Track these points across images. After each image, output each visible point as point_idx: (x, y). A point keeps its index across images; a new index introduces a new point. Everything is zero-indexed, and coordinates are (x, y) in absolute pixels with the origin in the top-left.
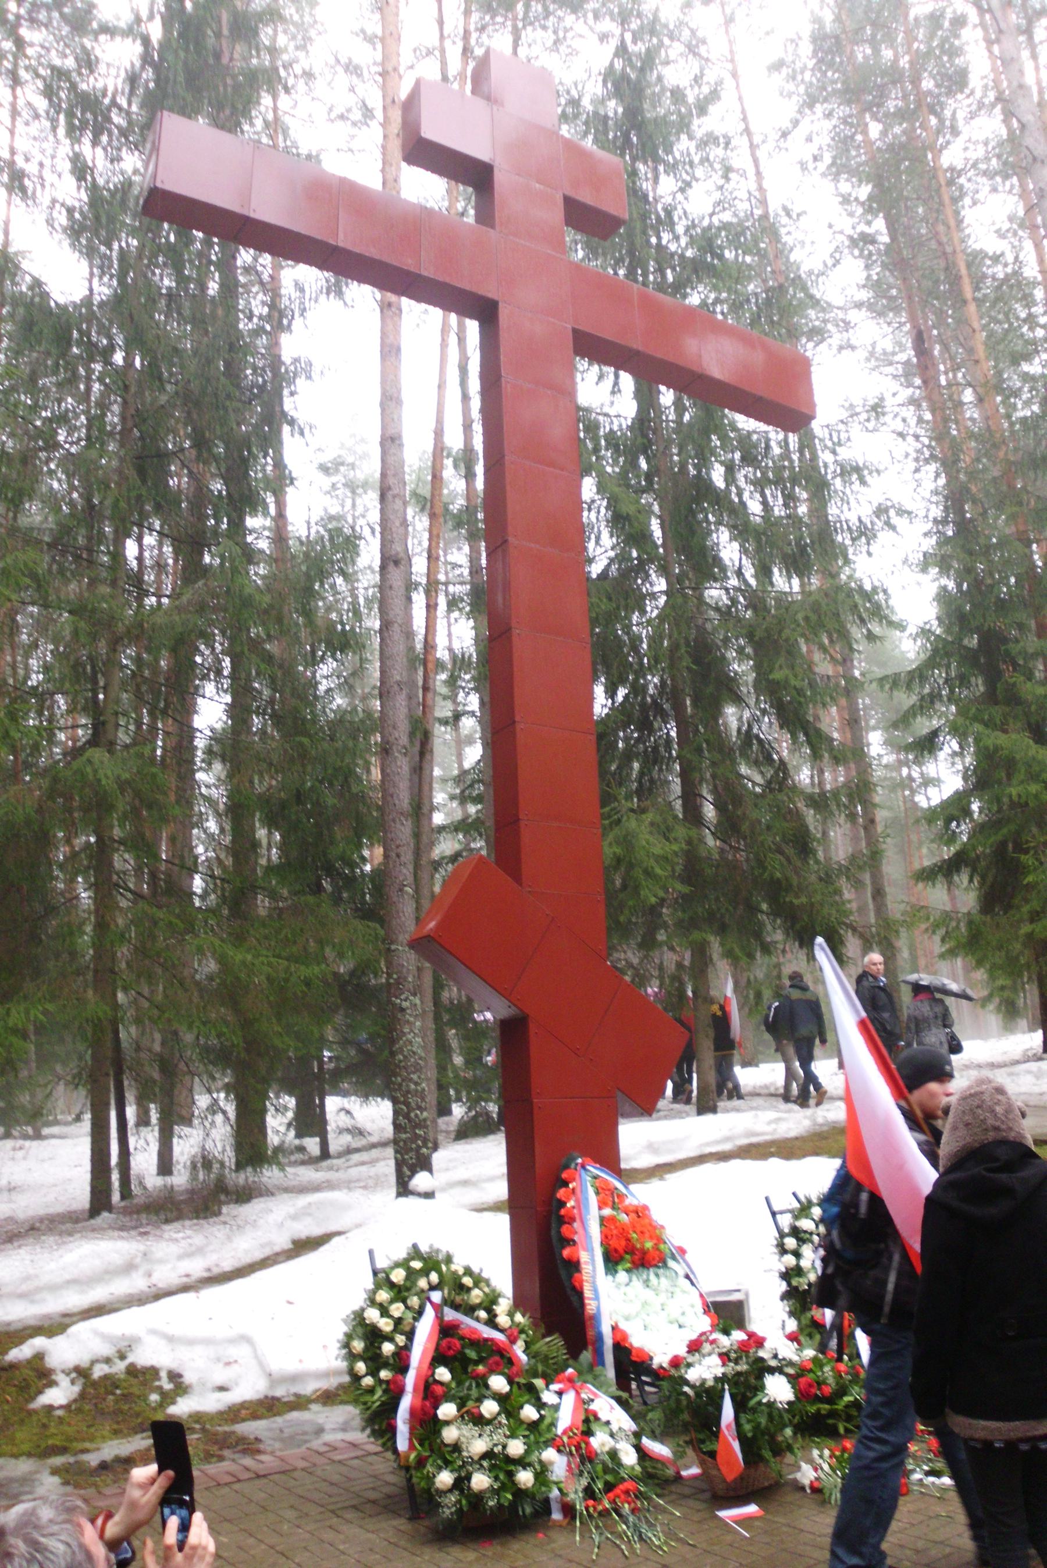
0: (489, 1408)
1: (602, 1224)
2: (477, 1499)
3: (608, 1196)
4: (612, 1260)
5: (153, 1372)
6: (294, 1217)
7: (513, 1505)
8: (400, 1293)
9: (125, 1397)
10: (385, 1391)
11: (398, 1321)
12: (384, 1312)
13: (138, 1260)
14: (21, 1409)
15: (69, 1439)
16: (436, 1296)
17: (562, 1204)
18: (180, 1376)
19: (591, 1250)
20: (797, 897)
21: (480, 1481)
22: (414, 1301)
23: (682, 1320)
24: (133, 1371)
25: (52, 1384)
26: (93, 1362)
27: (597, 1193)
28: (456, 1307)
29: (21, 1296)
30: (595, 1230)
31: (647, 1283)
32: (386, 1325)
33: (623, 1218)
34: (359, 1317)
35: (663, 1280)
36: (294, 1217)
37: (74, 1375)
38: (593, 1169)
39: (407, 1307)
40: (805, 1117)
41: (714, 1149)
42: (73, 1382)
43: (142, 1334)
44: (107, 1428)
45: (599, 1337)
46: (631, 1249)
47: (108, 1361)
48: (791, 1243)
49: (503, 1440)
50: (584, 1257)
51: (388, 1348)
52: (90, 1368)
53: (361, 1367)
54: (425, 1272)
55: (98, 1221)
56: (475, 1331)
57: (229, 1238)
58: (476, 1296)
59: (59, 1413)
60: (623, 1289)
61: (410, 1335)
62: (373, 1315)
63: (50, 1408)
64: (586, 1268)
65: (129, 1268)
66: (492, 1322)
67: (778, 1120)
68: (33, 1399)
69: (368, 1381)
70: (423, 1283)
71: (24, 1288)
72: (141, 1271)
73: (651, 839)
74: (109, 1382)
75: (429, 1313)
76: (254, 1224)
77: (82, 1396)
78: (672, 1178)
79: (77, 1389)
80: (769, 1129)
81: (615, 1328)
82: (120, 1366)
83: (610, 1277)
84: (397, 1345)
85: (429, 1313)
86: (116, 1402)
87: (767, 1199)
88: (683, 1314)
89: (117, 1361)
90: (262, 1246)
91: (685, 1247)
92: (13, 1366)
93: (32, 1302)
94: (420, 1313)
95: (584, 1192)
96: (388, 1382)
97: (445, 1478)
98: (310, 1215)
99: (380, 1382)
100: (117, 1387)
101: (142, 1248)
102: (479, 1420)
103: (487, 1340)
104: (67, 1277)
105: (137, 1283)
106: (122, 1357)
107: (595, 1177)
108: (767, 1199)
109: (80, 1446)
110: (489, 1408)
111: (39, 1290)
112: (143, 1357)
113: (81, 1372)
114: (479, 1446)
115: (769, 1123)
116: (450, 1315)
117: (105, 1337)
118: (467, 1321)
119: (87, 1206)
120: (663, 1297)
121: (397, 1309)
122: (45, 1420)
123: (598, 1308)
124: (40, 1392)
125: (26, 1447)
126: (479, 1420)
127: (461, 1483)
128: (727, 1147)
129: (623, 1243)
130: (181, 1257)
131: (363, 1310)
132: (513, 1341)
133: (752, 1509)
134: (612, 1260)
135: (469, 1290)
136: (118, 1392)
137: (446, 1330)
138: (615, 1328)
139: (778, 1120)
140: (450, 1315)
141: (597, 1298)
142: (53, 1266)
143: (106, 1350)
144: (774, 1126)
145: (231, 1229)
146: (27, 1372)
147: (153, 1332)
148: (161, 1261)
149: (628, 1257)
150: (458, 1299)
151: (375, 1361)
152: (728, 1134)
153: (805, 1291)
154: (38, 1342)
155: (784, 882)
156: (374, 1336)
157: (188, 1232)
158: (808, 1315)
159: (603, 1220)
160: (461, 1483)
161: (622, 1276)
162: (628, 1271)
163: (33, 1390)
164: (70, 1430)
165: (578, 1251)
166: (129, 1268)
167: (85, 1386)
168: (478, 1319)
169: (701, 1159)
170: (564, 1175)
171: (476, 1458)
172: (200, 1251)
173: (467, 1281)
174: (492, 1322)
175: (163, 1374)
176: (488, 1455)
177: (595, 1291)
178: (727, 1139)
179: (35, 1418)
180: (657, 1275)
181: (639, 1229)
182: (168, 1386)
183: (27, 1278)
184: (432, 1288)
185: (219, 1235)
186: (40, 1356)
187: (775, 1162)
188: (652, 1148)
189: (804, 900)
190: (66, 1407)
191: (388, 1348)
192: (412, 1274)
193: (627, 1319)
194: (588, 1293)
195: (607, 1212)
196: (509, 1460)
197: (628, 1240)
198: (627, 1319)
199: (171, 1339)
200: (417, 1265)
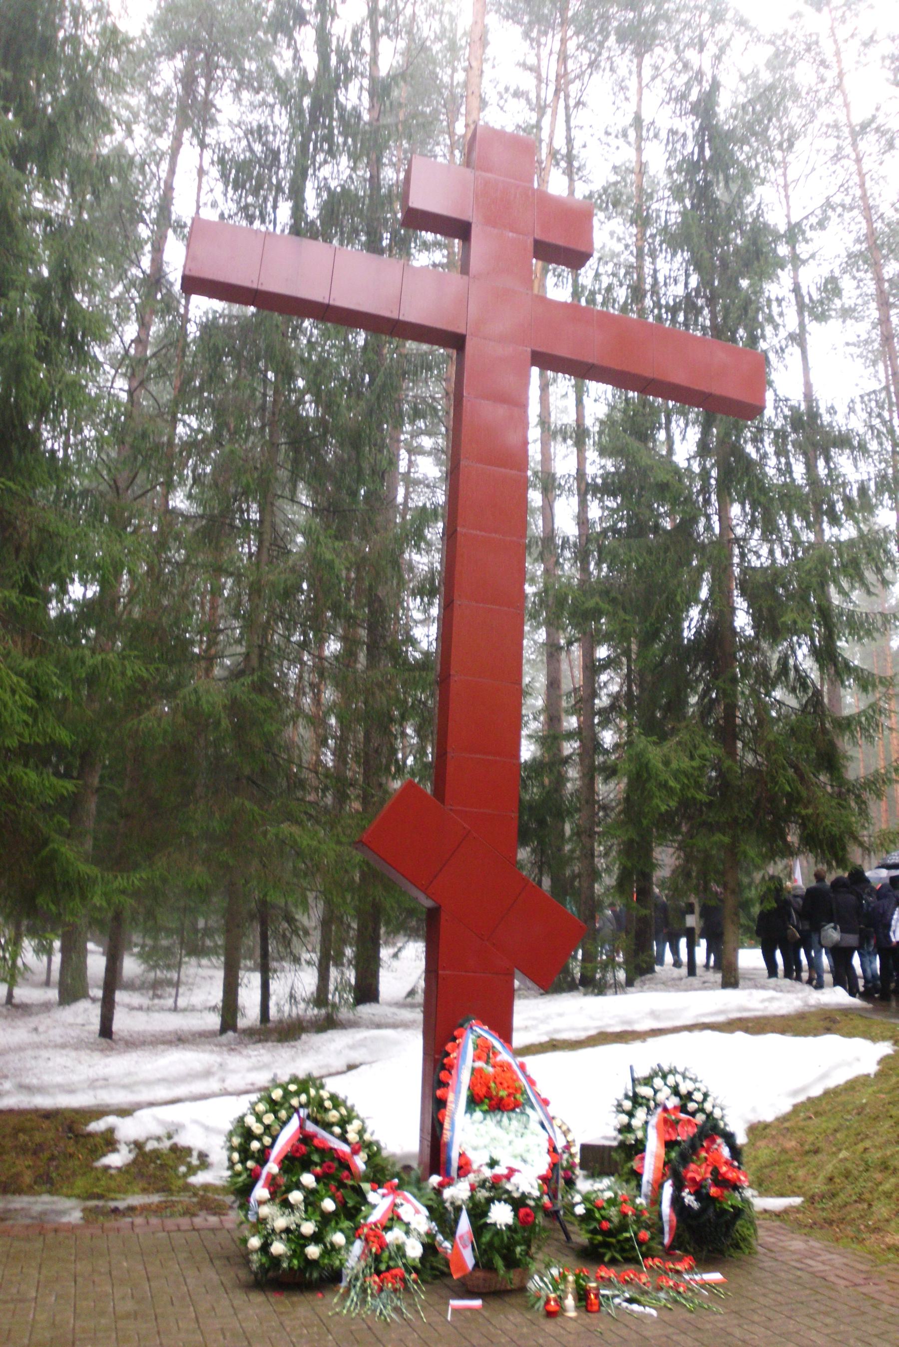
0: (296, 1197)
1: (472, 1073)
2: (276, 1260)
3: (484, 1052)
4: (474, 1102)
5: (188, 1151)
6: (352, 1047)
7: (302, 1271)
8: (274, 1106)
9: (162, 1166)
10: (249, 1176)
11: (267, 1128)
12: (259, 1119)
13: (215, 1069)
14: (87, 1166)
15: (109, 1190)
16: (303, 1112)
17: (448, 1054)
18: (207, 1156)
19: (457, 1094)
20: (806, 807)
21: (278, 1248)
22: (283, 1114)
23: (525, 1155)
24: (175, 1148)
25: (115, 1150)
26: (148, 1139)
27: (475, 1049)
28: (316, 1122)
29: (125, 1087)
30: (465, 1077)
31: (499, 1122)
32: (257, 1129)
33: (490, 1070)
34: (241, 1120)
35: (514, 1123)
36: (352, 1047)
37: (132, 1146)
38: (482, 1031)
39: (277, 1117)
40: (797, 998)
41: (707, 1020)
42: (130, 1151)
43: (186, 1122)
44: (143, 1184)
45: (449, 1161)
46: (488, 1095)
47: (159, 1139)
48: (628, 1105)
49: (298, 1221)
50: (451, 1097)
51: (255, 1145)
52: (145, 1143)
53: (236, 1156)
54: (297, 1094)
55: (224, 1039)
56: (323, 1141)
57: (293, 1059)
58: (333, 1116)
59: (113, 1172)
60: (477, 1125)
61: (274, 1139)
62: (250, 1121)
63: (107, 1168)
64: (450, 1106)
65: (207, 1074)
66: (343, 1138)
67: (771, 999)
68: (98, 1159)
69: (239, 1167)
70: (294, 1102)
71: (126, 1081)
72: (216, 1078)
73: (137, 879)
74: (156, 1154)
75: (295, 1123)
76: (318, 1051)
77: (134, 1162)
78: (651, 1041)
79: (131, 1156)
80: (761, 1006)
81: (462, 1155)
82: (167, 1144)
83: (468, 1115)
84: (263, 1144)
85: (295, 1123)
86: (155, 1168)
87: (631, 1067)
88: (528, 1151)
89: (165, 1140)
90: (320, 1067)
91: (549, 1098)
92: (90, 1135)
93: (132, 1092)
94: (284, 1123)
95: (466, 1047)
96: (251, 1170)
97: (255, 1242)
98: (365, 1046)
99: (246, 1169)
100: (158, 1158)
101: (219, 1059)
102: (286, 1204)
103: (331, 1149)
104: (159, 1076)
105: (213, 1085)
106: (170, 1137)
107: (479, 1036)
108: (631, 1067)
109: (112, 1195)
110: (296, 1197)
111: (136, 1083)
112: (183, 1140)
113: (138, 1145)
114: (281, 1223)
115: (763, 1001)
116: (310, 1127)
117: (161, 1122)
118: (322, 1133)
119: (218, 1027)
120: (512, 1136)
121: (269, 1119)
122: (100, 1175)
123: (452, 1137)
124: (104, 1155)
125: (77, 1191)
126: (286, 1204)
127: (265, 1247)
128: (721, 1018)
129: (484, 1090)
130: (250, 1070)
131: (245, 1115)
132: (355, 1152)
133: (477, 1303)
134: (474, 1102)
135: (326, 1110)
136: (159, 1162)
137: (305, 1138)
138: (462, 1155)
139: (771, 999)
140: (310, 1127)
141: (452, 1130)
142: (149, 1066)
143: (160, 1131)
144: (766, 1004)
145: (296, 1053)
146: (98, 1140)
147: (196, 1122)
148: (233, 1071)
149: (487, 1101)
150: (319, 1117)
151: (245, 1153)
152: (722, 1007)
153: (631, 1145)
154: (111, 1120)
155: (795, 795)
156: (248, 1135)
157: (262, 1051)
158: (629, 1165)
159: (474, 1070)
160: (265, 1247)
161: (478, 1115)
162: (485, 1112)
163: (100, 1152)
164: (113, 1184)
165: (447, 1093)
166: (207, 1074)
167: (137, 1155)
168: (332, 1133)
169: (690, 1028)
170: (456, 1033)
171: (278, 1231)
172: (266, 1066)
173: (328, 1104)
174: (343, 1138)
175: (195, 1154)
176: (287, 1230)
177: (452, 1124)
178: (721, 1012)
179: (93, 1173)
180: (510, 1119)
181: (498, 1080)
182: (195, 1161)
183: (129, 1074)
184: (301, 1106)
185: (284, 1055)
186: (111, 1130)
187: (740, 1035)
188: (653, 1014)
189: (810, 811)
190: (119, 1169)
191: (255, 1145)
192: (287, 1094)
193: (475, 1149)
194: (446, 1125)
195: (480, 1064)
196: (302, 1236)
197: (489, 1088)
198: (475, 1149)
199: (207, 1129)
200: (293, 1088)
